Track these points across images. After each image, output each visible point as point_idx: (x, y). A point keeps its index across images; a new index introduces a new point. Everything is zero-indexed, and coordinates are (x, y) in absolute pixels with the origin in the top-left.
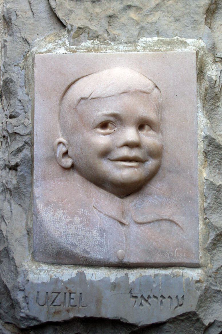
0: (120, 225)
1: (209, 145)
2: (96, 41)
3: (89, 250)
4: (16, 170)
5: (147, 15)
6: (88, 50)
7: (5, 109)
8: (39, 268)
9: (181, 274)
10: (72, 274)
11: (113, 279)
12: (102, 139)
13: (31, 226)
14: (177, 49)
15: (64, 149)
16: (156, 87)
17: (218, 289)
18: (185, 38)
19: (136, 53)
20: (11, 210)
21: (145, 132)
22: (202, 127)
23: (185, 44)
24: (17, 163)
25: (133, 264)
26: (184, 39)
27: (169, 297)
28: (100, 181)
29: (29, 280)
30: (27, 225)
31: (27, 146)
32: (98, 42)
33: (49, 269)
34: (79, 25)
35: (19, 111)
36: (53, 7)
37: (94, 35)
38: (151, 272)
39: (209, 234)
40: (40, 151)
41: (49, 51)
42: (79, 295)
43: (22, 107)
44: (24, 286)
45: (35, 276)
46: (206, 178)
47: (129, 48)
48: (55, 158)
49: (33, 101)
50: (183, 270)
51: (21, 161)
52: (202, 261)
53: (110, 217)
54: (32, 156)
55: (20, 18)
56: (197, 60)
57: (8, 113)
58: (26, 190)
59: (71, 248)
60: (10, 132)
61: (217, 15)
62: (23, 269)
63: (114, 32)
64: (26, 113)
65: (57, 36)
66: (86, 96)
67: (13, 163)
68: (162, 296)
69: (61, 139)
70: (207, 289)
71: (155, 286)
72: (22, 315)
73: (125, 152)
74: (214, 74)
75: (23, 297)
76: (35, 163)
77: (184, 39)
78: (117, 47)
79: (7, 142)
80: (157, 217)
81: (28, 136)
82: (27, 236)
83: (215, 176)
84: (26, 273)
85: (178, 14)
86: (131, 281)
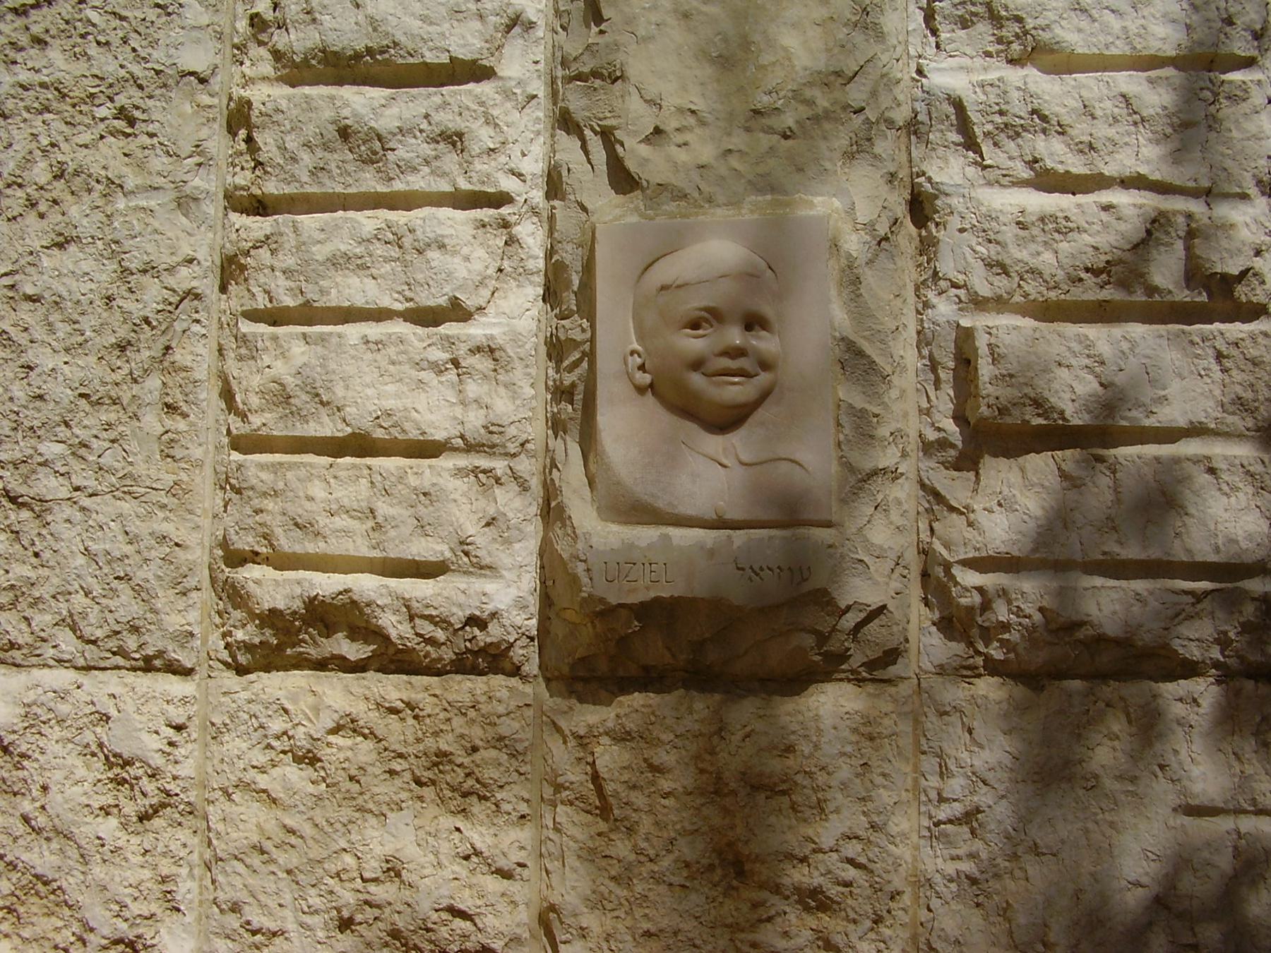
2: (683, 203)
6: (672, 216)
15: (639, 361)
40: (607, 364)
59: (650, 500)
66: (669, 283)
86: (735, 546)
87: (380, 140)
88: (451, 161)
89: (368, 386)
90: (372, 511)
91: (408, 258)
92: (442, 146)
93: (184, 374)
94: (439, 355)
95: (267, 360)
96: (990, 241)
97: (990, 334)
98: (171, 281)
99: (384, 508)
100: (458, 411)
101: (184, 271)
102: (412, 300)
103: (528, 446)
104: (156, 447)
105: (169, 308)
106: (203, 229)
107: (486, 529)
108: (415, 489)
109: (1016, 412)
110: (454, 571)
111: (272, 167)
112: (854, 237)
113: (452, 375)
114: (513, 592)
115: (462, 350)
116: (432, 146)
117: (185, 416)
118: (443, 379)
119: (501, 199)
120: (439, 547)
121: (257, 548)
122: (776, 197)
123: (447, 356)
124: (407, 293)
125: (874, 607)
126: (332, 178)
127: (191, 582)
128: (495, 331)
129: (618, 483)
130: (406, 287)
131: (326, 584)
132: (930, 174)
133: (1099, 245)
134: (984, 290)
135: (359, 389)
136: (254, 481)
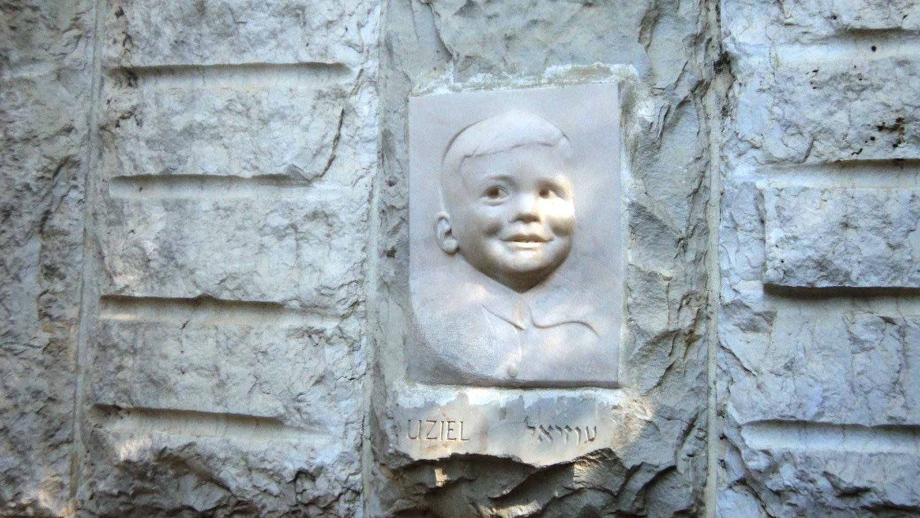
2: (489, 75)
3: (472, 364)
5: (559, 33)
6: (477, 87)
15: (447, 227)
16: (564, 135)
18: (610, 62)
22: (627, 190)
23: (607, 72)
26: (608, 65)
28: (490, 270)
34: (467, 53)
37: (487, 66)
38: (554, 394)
39: (635, 342)
40: (418, 229)
48: (437, 239)
57: (387, 178)
59: (451, 361)
61: (661, 25)
62: (393, 389)
63: (512, 59)
66: (470, 153)
67: (389, 248)
68: (567, 427)
69: (444, 213)
72: (390, 451)
74: (649, 113)
77: (608, 65)
85: (600, 28)
86: (526, 406)
87: (232, 13)
88: (294, 34)
90: (217, 369)
91: (254, 128)
93: (61, 238)
95: (131, 224)
96: (786, 102)
97: (778, 195)
98: (49, 149)
99: (227, 368)
100: (295, 274)
101: (63, 140)
103: (361, 308)
104: (34, 307)
105: (48, 175)
106: (81, 99)
107: (317, 388)
108: (255, 348)
109: (800, 274)
110: (288, 427)
111: (141, 40)
112: (650, 103)
114: (338, 448)
115: (299, 217)
116: (278, 19)
117: (62, 277)
118: (284, 243)
119: (339, 68)
121: (118, 403)
122: (576, 66)
123: (286, 222)
124: (254, 162)
125: (662, 468)
126: (190, 51)
127: (62, 435)
128: (331, 197)
129: (424, 344)
130: (252, 156)
131: (174, 437)
132: (734, 34)
133: (891, 103)
134: (780, 153)
135: (209, 253)
136: (116, 340)
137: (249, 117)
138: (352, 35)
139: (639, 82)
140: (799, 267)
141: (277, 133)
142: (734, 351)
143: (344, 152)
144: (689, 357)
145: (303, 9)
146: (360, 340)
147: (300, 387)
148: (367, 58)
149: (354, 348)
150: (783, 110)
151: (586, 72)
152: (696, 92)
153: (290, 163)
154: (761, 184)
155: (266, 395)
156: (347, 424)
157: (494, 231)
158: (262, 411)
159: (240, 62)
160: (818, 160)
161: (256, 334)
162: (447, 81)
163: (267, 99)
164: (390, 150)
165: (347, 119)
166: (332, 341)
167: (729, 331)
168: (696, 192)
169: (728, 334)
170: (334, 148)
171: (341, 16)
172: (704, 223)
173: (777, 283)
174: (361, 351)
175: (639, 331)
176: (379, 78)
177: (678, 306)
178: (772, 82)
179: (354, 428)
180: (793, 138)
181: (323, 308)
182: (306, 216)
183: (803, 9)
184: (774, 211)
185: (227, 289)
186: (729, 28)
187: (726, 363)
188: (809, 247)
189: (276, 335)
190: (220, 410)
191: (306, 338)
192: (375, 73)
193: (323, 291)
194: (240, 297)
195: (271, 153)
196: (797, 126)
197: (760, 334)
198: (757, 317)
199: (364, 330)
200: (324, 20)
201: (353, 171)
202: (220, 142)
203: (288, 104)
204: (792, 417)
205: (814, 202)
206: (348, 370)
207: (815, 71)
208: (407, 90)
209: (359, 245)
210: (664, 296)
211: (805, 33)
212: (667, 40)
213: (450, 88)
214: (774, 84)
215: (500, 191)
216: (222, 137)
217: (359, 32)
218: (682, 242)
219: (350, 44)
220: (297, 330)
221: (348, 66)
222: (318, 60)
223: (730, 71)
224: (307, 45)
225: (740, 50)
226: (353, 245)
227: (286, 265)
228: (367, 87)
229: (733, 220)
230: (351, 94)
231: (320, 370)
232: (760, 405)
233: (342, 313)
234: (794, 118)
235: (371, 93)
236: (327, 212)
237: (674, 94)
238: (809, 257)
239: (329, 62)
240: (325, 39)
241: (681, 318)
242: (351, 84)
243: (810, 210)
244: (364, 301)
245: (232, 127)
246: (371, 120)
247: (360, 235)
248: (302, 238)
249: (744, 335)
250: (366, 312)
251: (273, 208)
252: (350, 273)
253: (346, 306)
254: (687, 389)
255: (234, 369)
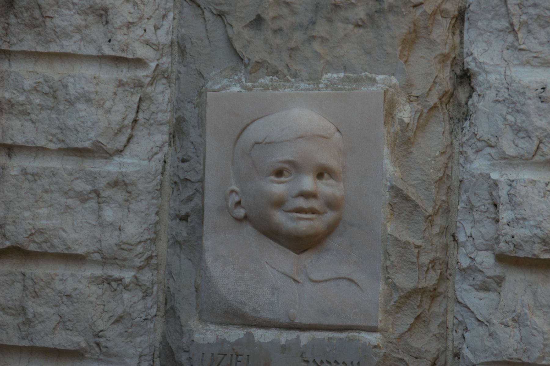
0: (293, 282)
1: (396, 196)
2: (275, 78)
4: (187, 221)
6: (265, 88)
7: (178, 150)
8: (205, 328)
9: (358, 337)
10: (239, 334)
11: (283, 341)
12: (277, 188)
13: (199, 282)
14: (362, 88)
15: (237, 199)
16: (338, 130)
17: (400, 357)
18: (375, 74)
19: (317, 92)
20: (180, 265)
21: (324, 181)
23: (373, 81)
24: (187, 213)
25: (305, 325)
26: (374, 75)
27: (344, 363)
28: (274, 234)
29: (194, 340)
30: (195, 281)
31: (198, 195)
32: (277, 79)
33: (216, 329)
34: (257, 59)
35: (191, 154)
36: (230, 36)
39: (391, 295)
40: (211, 200)
41: (223, 88)
42: (246, 357)
43: (194, 151)
44: (188, 347)
45: (201, 336)
46: (390, 233)
47: (311, 87)
48: (227, 208)
49: (204, 144)
50: (359, 333)
51: (192, 211)
52: (380, 325)
53: (283, 273)
54: (203, 205)
55: (195, 46)
56: (385, 100)
57: (180, 155)
58: (196, 243)
60: (182, 177)
64: (198, 157)
65: (235, 70)
66: (260, 140)
67: (183, 213)
68: (336, 362)
69: (234, 187)
70: (386, 356)
71: (328, 350)
73: (301, 203)
75: (187, 359)
76: (205, 213)
77: (374, 75)
78: (297, 85)
79: (179, 189)
80: (335, 275)
81: (199, 183)
82: (196, 293)
83: (402, 231)
84: (191, 332)
86: (302, 344)
87: (40, 8)
88: (96, 31)
89: (25, 209)
90: (24, 309)
91: (61, 107)
92: (91, 18)
94: (82, 186)
96: (518, 111)
97: (510, 185)
99: (33, 307)
100: (97, 232)
102: (63, 141)
103: (154, 261)
107: (114, 326)
108: (60, 292)
112: (407, 107)
113: (92, 204)
115: (101, 184)
116: (83, 17)
118: (87, 206)
119: (139, 62)
120: (76, 339)
123: (89, 188)
124: (60, 136)
128: (130, 169)
130: (59, 131)
132: (476, 55)
134: (511, 151)
137: (55, 98)
138: (150, 35)
139: (399, 90)
140: (527, 242)
141: (83, 114)
142: (469, 306)
143: (141, 133)
144: (432, 309)
145: (106, 10)
146: (153, 287)
147: (101, 325)
148: (162, 55)
149: (146, 294)
150: (515, 118)
151: (357, 81)
152: (444, 99)
153: (94, 139)
154: (495, 176)
155: (69, 332)
156: (141, 356)
157: (279, 203)
158: (66, 345)
159: (46, 51)
160: (543, 159)
161: (61, 280)
162: (239, 81)
163: (73, 84)
164: (183, 133)
165: (144, 105)
166: (129, 288)
167: (465, 290)
168: (441, 179)
169: (464, 292)
170: (132, 129)
171: (141, 18)
172: (446, 204)
173: (508, 254)
174: (152, 297)
175: (393, 287)
176: (172, 72)
177: (426, 269)
178: (506, 95)
179: (146, 360)
180: (522, 140)
181: (121, 260)
182: (108, 184)
183: (535, 38)
184: (507, 197)
185: (35, 242)
186: (471, 49)
187: (462, 316)
188: (536, 226)
189: (80, 282)
190: (25, 343)
191: (106, 285)
192: (168, 68)
193: (123, 246)
194: (47, 249)
195: (77, 130)
196: (526, 131)
197: (491, 293)
198: (489, 280)
199: (155, 279)
200: (125, 21)
201: (149, 148)
202: (28, 117)
203: (92, 89)
204: (518, 359)
205: (539, 192)
206: (142, 312)
207: (543, 88)
208: (201, 85)
209: (154, 209)
210: (416, 260)
211: (535, 57)
212: (421, 57)
213: (242, 87)
214: (508, 97)
215: (285, 172)
216: (29, 113)
217: (156, 34)
218: (430, 218)
219: (148, 43)
220: (97, 278)
221: (146, 60)
222: (120, 54)
223: (470, 84)
224: (110, 41)
225: (479, 68)
226: (148, 209)
227: (89, 223)
228: (160, 79)
229: (470, 202)
230: (148, 84)
231: (120, 311)
232: (492, 349)
233: (138, 264)
234: (524, 125)
235: (164, 84)
236: (127, 182)
237: (426, 101)
238: (535, 234)
239: (130, 56)
240: (126, 37)
241: (428, 278)
242: (147, 76)
243: (537, 198)
244: (156, 256)
245: (39, 105)
246: (164, 107)
247: (154, 201)
248: (104, 202)
249: (477, 293)
250: (157, 264)
251: (78, 176)
252: (146, 232)
253: (142, 259)
254: (431, 335)
255: (40, 310)
